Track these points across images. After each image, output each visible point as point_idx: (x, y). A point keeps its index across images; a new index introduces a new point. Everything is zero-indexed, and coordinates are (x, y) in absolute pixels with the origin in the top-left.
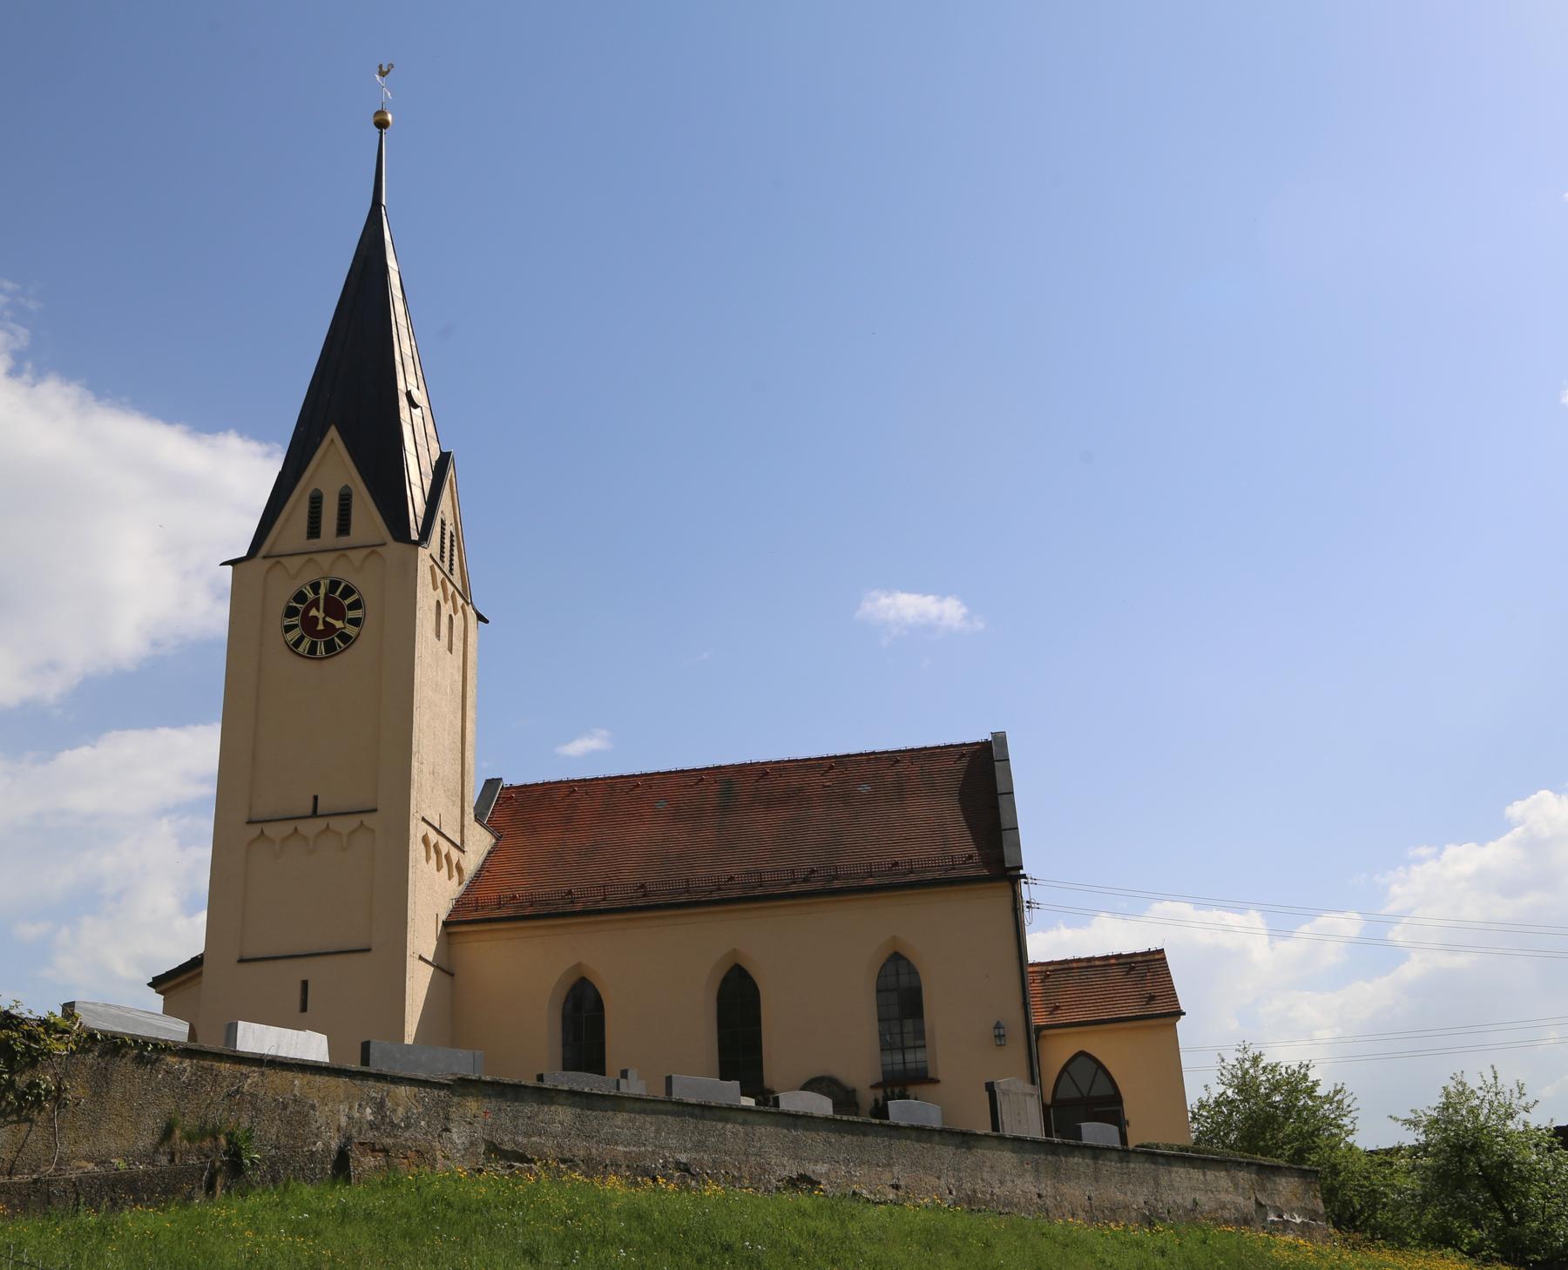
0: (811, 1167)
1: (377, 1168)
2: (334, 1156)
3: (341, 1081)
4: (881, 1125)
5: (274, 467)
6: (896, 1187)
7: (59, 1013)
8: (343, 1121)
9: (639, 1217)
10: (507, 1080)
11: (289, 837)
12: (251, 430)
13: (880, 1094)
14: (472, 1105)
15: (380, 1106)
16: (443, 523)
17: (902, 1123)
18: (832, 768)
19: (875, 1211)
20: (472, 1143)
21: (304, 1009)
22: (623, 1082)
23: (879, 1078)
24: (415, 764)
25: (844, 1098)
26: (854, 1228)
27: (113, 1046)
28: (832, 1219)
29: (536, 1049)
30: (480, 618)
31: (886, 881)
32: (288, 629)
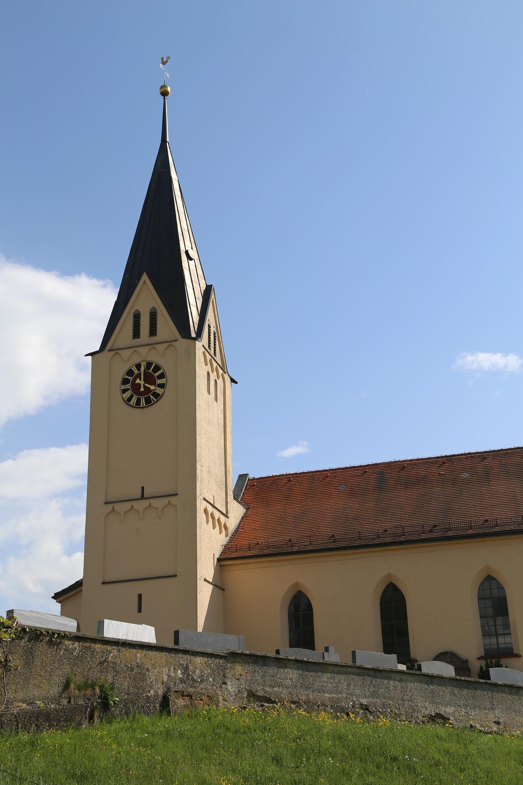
0: (444, 709)
1: (186, 706)
2: (160, 699)
3: (164, 654)
4: (485, 683)
5: (114, 298)
6: (498, 723)
7: (5, 616)
8: (165, 678)
9: (340, 738)
10: (258, 653)
11: (128, 511)
12: (96, 273)
13: (483, 663)
14: (239, 669)
15: (186, 669)
16: (209, 326)
17: (499, 682)
18: (444, 463)
19: (485, 738)
20: (239, 692)
21: (140, 611)
22: (326, 654)
23: (483, 654)
24: (198, 467)
25: (461, 666)
26: (472, 749)
27: (35, 635)
28: (458, 743)
29: (274, 635)
30: (233, 381)
31: (481, 531)
32: (124, 391)
